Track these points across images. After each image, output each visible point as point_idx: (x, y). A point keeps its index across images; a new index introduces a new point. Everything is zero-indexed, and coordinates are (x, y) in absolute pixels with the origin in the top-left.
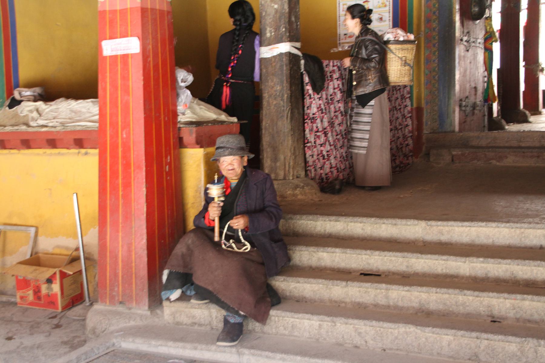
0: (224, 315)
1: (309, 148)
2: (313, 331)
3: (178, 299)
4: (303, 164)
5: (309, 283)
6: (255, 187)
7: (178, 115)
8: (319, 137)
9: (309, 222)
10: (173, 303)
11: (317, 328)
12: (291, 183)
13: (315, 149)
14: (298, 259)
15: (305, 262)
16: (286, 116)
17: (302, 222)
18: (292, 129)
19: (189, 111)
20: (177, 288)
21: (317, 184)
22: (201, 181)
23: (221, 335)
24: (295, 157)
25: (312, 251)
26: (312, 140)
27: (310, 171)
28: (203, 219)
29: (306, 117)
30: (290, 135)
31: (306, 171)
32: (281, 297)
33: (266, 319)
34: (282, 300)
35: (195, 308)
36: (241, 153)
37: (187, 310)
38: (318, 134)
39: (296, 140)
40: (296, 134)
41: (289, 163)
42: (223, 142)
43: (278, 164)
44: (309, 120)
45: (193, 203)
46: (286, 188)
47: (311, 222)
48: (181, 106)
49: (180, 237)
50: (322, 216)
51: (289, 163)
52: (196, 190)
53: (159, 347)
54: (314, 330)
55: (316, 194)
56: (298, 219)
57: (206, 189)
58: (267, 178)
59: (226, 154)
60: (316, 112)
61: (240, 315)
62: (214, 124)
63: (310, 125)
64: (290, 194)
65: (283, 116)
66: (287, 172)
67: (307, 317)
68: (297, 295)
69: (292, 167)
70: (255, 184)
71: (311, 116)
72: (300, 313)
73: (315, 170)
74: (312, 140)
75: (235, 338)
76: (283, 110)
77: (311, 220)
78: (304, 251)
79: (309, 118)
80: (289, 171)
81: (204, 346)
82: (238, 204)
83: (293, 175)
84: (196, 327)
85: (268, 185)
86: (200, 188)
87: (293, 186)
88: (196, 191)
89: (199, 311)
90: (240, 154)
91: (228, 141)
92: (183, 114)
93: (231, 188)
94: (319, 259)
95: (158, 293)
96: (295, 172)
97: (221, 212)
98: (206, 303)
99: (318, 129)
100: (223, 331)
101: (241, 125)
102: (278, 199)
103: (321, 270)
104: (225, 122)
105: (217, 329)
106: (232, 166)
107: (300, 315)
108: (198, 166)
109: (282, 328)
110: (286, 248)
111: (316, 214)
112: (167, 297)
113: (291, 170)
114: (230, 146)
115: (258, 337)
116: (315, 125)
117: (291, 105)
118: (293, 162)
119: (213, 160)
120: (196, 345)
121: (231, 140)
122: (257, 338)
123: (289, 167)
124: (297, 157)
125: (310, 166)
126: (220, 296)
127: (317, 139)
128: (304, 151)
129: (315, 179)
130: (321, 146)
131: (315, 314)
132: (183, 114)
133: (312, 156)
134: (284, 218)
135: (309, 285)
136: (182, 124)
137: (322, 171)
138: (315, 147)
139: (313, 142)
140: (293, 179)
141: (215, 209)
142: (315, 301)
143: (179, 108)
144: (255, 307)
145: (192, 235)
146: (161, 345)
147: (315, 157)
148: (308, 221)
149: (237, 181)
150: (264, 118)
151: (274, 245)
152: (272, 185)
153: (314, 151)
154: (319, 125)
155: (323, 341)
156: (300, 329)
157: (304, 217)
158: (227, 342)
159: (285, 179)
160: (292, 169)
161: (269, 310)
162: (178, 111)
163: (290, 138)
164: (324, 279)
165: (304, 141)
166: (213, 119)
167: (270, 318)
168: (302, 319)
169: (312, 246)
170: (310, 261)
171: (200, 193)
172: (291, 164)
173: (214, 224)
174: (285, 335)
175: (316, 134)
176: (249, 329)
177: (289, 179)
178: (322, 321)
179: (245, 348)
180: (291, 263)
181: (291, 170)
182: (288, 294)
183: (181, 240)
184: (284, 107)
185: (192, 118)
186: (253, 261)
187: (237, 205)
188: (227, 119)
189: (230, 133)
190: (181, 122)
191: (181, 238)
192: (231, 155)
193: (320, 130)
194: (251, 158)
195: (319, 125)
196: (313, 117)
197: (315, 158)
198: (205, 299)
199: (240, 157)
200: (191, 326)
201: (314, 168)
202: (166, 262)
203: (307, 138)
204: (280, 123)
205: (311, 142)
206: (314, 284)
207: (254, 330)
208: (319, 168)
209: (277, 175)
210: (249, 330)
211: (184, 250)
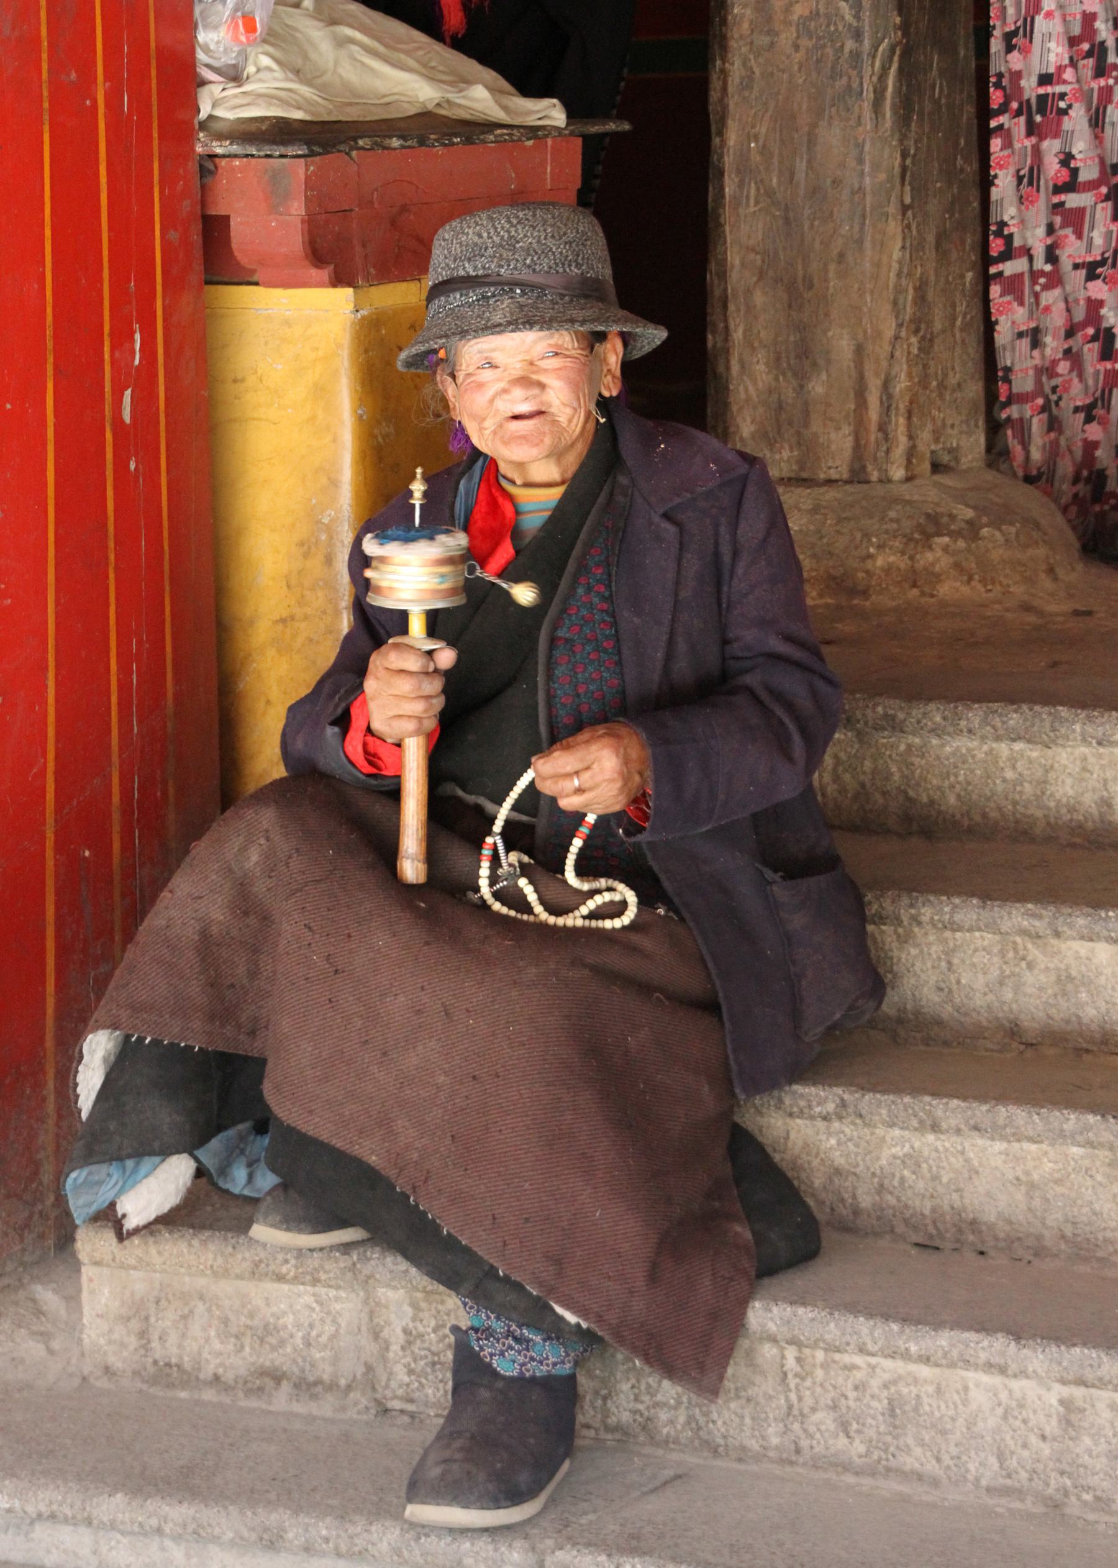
0: (455, 1329)
1: (1013, 285)
2: (1025, 1446)
3: (169, 1221)
4: (975, 389)
5: (996, 1132)
6: (670, 529)
7: (203, 83)
8: (1076, 220)
9: (1003, 749)
10: (136, 1240)
11: (1052, 1427)
12: (896, 500)
13: (1049, 298)
14: (933, 979)
15: (979, 1001)
16: (869, 94)
17: (963, 743)
18: (904, 169)
19: (265, 61)
20: (165, 1152)
21: (1065, 510)
22: (334, 483)
23: (432, 1458)
24: (927, 344)
25: (1023, 932)
26: (1036, 238)
27: (1022, 428)
28: (332, 731)
29: (996, 97)
30: (893, 209)
31: (994, 428)
32: (821, 1216)
33: (726, 1356)
34: (828, 1237)
35: (280, 1278)
36: (588, 313)
37: (225, 1288)
38: (1073, 200)
39: (931, 238)
40: (934, 206)
41: (886, 385)
42: (476, 252)
43: (817, 387)
44: (1018, 113)
45: (283, 621)
46: (867, 535)
47: (1018, 746)
48: (216, 28)
49: (195, 829)
50: (1083, 714)
51: (886, 385)
52: (301, 544)
53: (40, 1531)
54: (1034, 1440)
55: (1051, 571)
56: (935, 731)
57: (360, 561)
58: (744, 480)
59: (497, 318)
60: (1060, 69)
61: (556, 1330)
62: (422, 142)
63: (1023, 142)
64: (888, 570)
65: (852, 92)
66: (873, 435)
67: (983, 1356)
68: (927, 1207)
69: (902, 406)
70: (666, 516)
71: (1030, 87)
72: (938, 1325)
73: (1054, 424)
74: (1036, 238)
75: (523, 1478)
76: (856, 56)
77: (1019, 738)
78: (971, 930)
79: (1015, 105)
80: (882, 428)
81: (323, 1528)
82: (562, 633)
83: (911, 453)
84: (281, 1400)
85: (752, 527)
86: (330, 530)
87: (907, 525)
88: (306, 548)
89: (305, 1295)
90: (583, 323)
91: (511, 244)
92: (234, 76)
93: (516, 534)
94: (1065, 981)
95: (47, 1177)
96: (925, 436)
97: (439, 703)
98: (346, 1248)
99: (1075, 172)
100: (446, 1436)
101: (592, 147)
102: (809, 602)
103: (1080, 1052)
104: (491, 126)
105: (412, 1416)
106: (536, 391)
107: (944, 1340)
108: (321, 392)
109: (824, 1419)
110: (860, 905)
111: (1050, 699)
112: (100, 1201)
113: (899, 424)
114: (525, 275)
115: (669, 1473)
116: (1051, 147)
117: (905, 27)
118: (910, 376)
119: (409, 364)
120: (276, 1517)
121: (526, 237)
122: (665, 1483)
123: (887, 408)
124: (938, 346)
125: (1023, 398)
126: (432, 1207)
127: (1069, 231)
128: (986, 300)
129: (1051, 481)
130: (1091, 276)
131: (1033, 1337)
132: (234, 76)
133: (1035, 337)
134: (850, 722)
135: (999, 1146)
136: (220, 137)
137: (1094, 432)
138: (1055, 280)
139: (1039, 252)
140: (909, 479)
141: (405, 686)
142: (1040, 1252)
143: (202, 36)
144: (653, 1277)
145: (267, 817)
146: (53, 1516)
147: (1052, 345)
148: (998, 739)
149: (557, 492)
150: (733, 103)
151: (781, 891)
152: (777, 518)
153: (1047, 309)
154: (1081, 147)
155: (1091, 1517)
156: (944, 1433)
157: (974, 715)
158: (466, 1506)
159: (858, 476)
160: (901, 420)
161: (743, 1304)
162: (201, 56)
163: (894, 227)
164: (1093, 1109)
165: (985, 245)
166: (412, 111)
167: (750, 1354)
168: (952, 1365)
169: (1021, 898)
170: (1008, 995)
171: (329, 560)
172: (901, 384)
173: (400, 763)
174: (846, 1467)
175: (1056, 200)
176: (612, 1420)
177: (886, 480)
178: (1081, 1382)
179: (588, 1545)
180: (888, 1007)
181: (899, 424)
182: (866, 1201)
183: (201, 848)
184: (858, 35)
185: (283, 102)
186: (645, 989)
187: (553, 641)
188: (505, 108)
189: (519, 199)
190: (216, 126)
191: (198, 837)
192: (529, 323)
193: (1088, 173)
194: (647, 349)
195: (1081, 147)
196: (1042, 99)
197: (1048, 351)
198: (342, 1223)
199: (579, 336)
200: (249, 1392)
201: (1044, 408)
202: (102, 984)
203: (1003, 224)
204: (832, 136)
205: (1027, 252)
206: (1031, 1140)
207: (647, 1426)
208: (1077, 410)
209: (808, 449)
210: (617, 1428)
211: (217, 912)
